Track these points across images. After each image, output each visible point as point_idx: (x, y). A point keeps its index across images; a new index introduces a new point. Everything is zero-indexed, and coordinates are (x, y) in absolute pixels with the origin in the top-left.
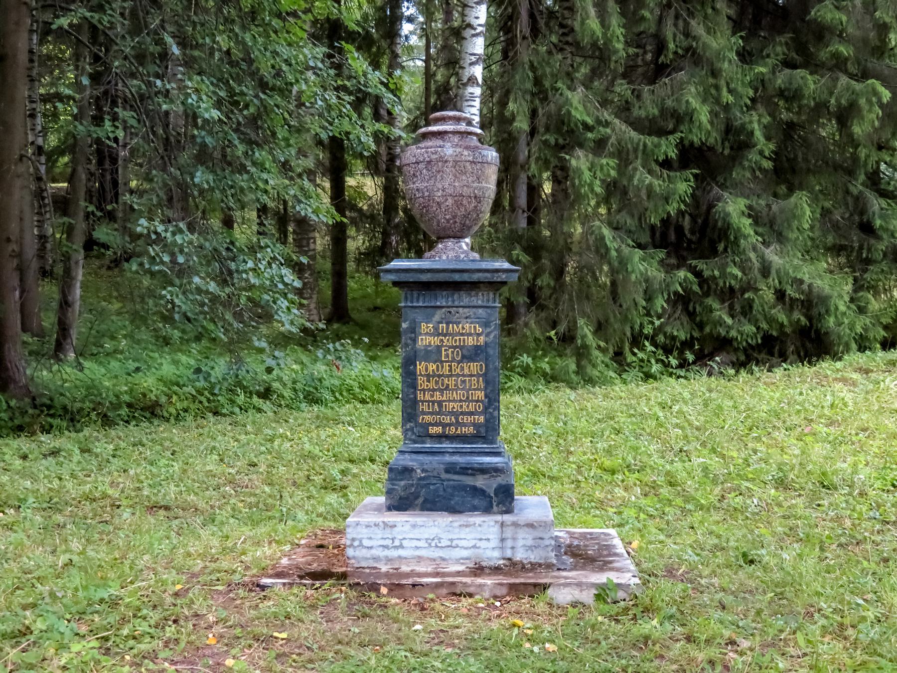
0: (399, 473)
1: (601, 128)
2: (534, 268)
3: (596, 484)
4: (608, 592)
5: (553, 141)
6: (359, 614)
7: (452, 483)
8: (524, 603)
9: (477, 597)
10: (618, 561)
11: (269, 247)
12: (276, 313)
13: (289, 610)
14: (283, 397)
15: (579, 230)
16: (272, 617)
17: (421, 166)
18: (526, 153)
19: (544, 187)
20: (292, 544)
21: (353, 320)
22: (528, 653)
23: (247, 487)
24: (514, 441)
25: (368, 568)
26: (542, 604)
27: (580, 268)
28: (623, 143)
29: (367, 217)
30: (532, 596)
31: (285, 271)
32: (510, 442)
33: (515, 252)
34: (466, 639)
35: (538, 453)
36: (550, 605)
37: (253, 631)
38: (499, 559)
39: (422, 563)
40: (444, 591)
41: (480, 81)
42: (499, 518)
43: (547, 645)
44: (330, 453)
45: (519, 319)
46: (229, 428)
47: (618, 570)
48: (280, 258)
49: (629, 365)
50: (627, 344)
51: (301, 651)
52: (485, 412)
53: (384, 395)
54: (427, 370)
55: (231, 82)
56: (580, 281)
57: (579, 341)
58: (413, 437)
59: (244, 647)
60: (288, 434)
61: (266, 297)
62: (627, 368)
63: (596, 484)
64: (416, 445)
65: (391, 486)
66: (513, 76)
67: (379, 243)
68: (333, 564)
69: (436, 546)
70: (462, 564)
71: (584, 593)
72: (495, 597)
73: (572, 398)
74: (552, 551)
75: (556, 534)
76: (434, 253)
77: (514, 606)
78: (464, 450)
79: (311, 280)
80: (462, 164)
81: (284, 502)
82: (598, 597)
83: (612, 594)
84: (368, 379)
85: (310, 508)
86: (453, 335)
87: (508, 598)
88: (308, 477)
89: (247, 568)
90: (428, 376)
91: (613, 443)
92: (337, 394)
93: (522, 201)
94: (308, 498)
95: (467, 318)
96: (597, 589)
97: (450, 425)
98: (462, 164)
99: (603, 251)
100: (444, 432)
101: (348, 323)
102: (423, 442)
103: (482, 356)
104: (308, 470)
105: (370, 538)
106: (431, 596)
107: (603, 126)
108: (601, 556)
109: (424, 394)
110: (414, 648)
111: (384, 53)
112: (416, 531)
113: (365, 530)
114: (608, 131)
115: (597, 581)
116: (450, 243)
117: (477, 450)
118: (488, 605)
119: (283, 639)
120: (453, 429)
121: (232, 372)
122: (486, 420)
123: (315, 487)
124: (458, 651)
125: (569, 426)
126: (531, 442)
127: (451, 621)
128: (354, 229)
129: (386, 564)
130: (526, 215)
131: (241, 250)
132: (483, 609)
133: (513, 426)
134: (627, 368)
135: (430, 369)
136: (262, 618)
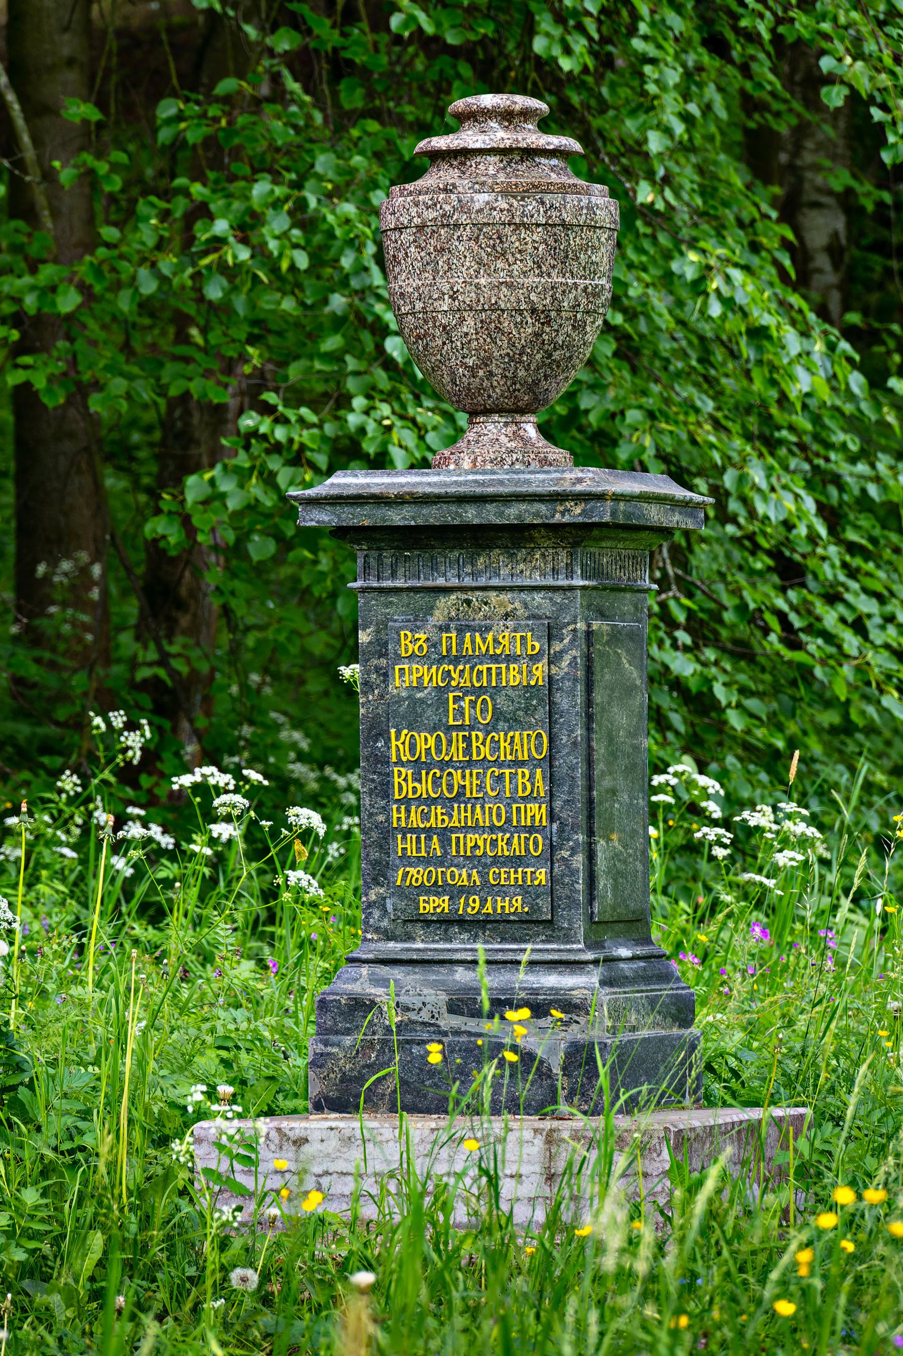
0: (342, 1014)
7: (464, 1039)
17: (406, 237)
54: (413, 748)
58: (385, 923)
64: (391, 945)
65: (320, 1048)
95: (507, 616)
102: (410, 938)
109: (408, 811)
120: (475, 902)
135: (421, 746)
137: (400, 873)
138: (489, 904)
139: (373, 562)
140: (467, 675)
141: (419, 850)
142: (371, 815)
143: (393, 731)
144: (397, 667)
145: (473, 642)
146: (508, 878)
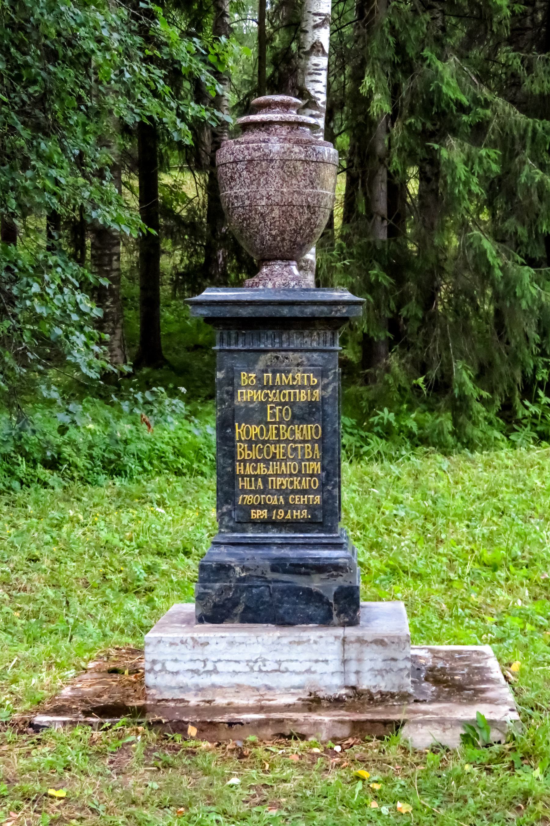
0: (213, 571)
1: (479, 110)
2: (397, 293)
3: (472, 584)
4: (478, 731)
5: (419, 127)
6: (160, 764)
7: (280, 585)
8: (371, 747)
9: (312, 739)
10: (492, 690)
11: (59, 266)
12: (70, 353)
13: (69, 758)
14: (76, 467)
15: (455, 242)
16: (48, 769)
17: (240, 166)
18: (386, 142)
19: (409, 186)
20: (77, 669)
21: (166, 362)
22: (374, 816)
23: (25, 590)
24: (369, 526)
25: (173, 700)
26: (393, 748)
27: (457, 293)
28: (507, 129)
29: (186, 226)
30: (380, 738)
31: (80, 297)
32: (364, 527)
33: (373, 272)
34: (296, 797)
35: (399, 542)
36: (405, 750)
37: (22, 788)
38: (340, 687)
39: (242, 694)
40: (269, 732)
41: (327, 48)
42: (340, 632)
43: (399, 805)
44: (134, 543)
45: (379, 361)
46: (5, 509)
47: (492, 701)
48: (74, 280)
49: (518, 422)
50: (517, 393)
51: (83, 814)
52: (322, 489)
53: (205, 464)
55: (12, 50)
56: (456, 311)
57: (456, 391)
58: (231, 524)
59: (10, 809)
60: (81, 517)
61: (58, 331)
62: (515, 426)
63: (472, 584)
64: (235, 535)
65: (202, 590)
66: (369, 42)
67: (202, 260)
68: (128, 696)
69: (260, 671)
70: (293, 694)
71: (447, 732)
72: (335, 740)
73: (445, 467)
74: (408, 676)
75: (413, 652)
76: (257, 280)
77: (358, 751)
78: (295, 541)
79: (114, 310)
80: (291, 164)
81: (72, 609)
82: (466, 739)
83: (483, 735)
84: (185, 442)
85: (104, 618)
86: (281, 388)
87: (351, 741)
88: (104, 575)
89: (18, 701)
90: (250, 442)
91: (495, 528)
92: (145, 463)
93: (382, 206)
94: (104, 604)
95: (298, 365)
96: (464, 728)
97: (277, 507)
98: (291, 164)
99: (484, 270)
100: (270, 517)
101: (161, 366)
102: (244, 531)
103: (320, 414)
104: (104, 567)
105: (176, 660)
106: (252, 738)
107: (482, 107)
108: (471, 683)
110: (228, 809)
111: (208, 11)
112: (235, 650)
113: (169, 650)
114: (489, 112)
115: (465, 718)
116: (277, 267)
117: (312, 541)
118: (326, 750)
119: (60, 799)
121: (14, 433)
122: (324, 501)
123: (113, 589)
124: (285, 814)
125: (439, 504)
126: (391, 527)
127: (277, 773)
128: (170, 241)
129: (196, 695)
130: (385, 223)
131: (23, 270)
132: (318, 755)
133: (368, 506)
134: (515, 426)
135: (252, 433)
136: (34, 770)
137: (241, 497)
138: (289, 514)
139: (225, 336)
140: (277, 395)
141: (251, 486)
142: (224, 468)
143: (237, 424)
144: (239, 391)
145: (281, 378)
146: (300, 501)
